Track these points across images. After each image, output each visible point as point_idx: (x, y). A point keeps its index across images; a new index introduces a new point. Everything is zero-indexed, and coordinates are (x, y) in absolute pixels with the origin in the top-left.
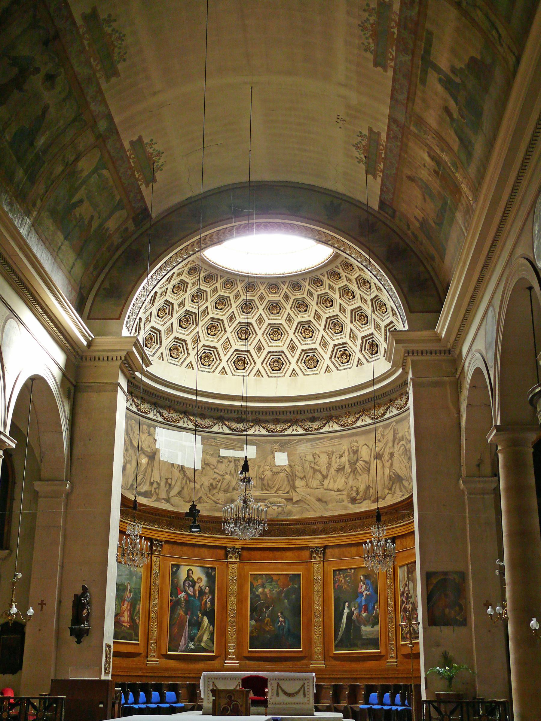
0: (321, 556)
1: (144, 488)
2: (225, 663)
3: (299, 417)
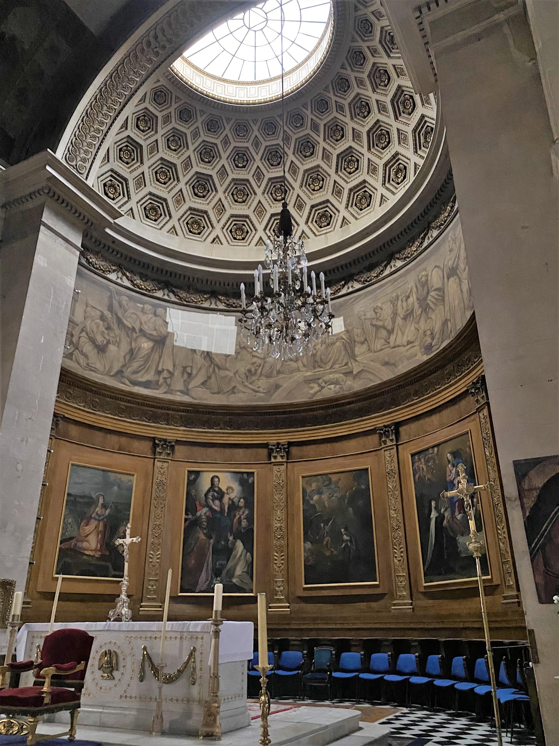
0: (394, 437)
2: (141, 607)
3: (354, 270)
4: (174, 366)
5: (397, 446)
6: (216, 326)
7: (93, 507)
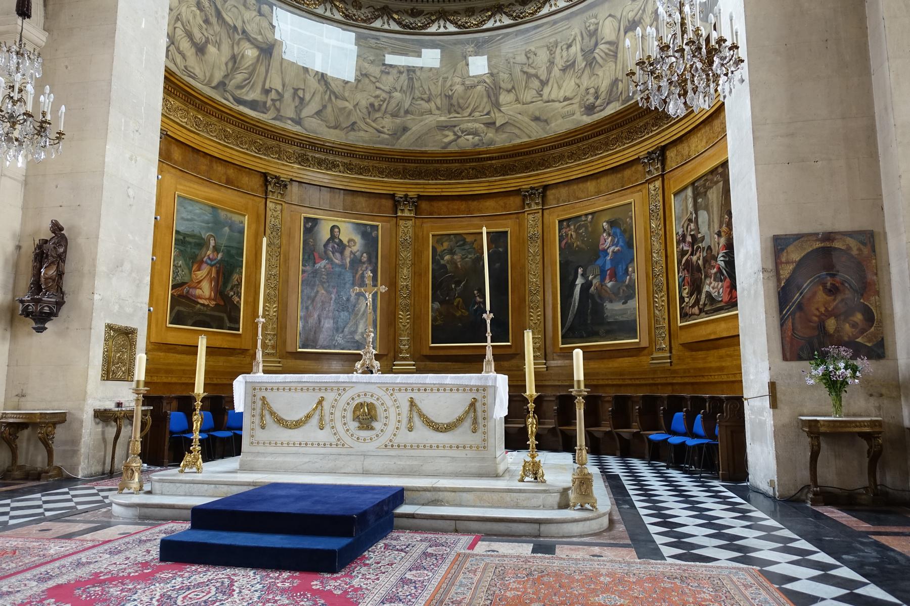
0: (540, 200)
1: (254, 95)
4: (284, 86)
5: (543, 210)
6: (333, 42)
7: (204, 249)
